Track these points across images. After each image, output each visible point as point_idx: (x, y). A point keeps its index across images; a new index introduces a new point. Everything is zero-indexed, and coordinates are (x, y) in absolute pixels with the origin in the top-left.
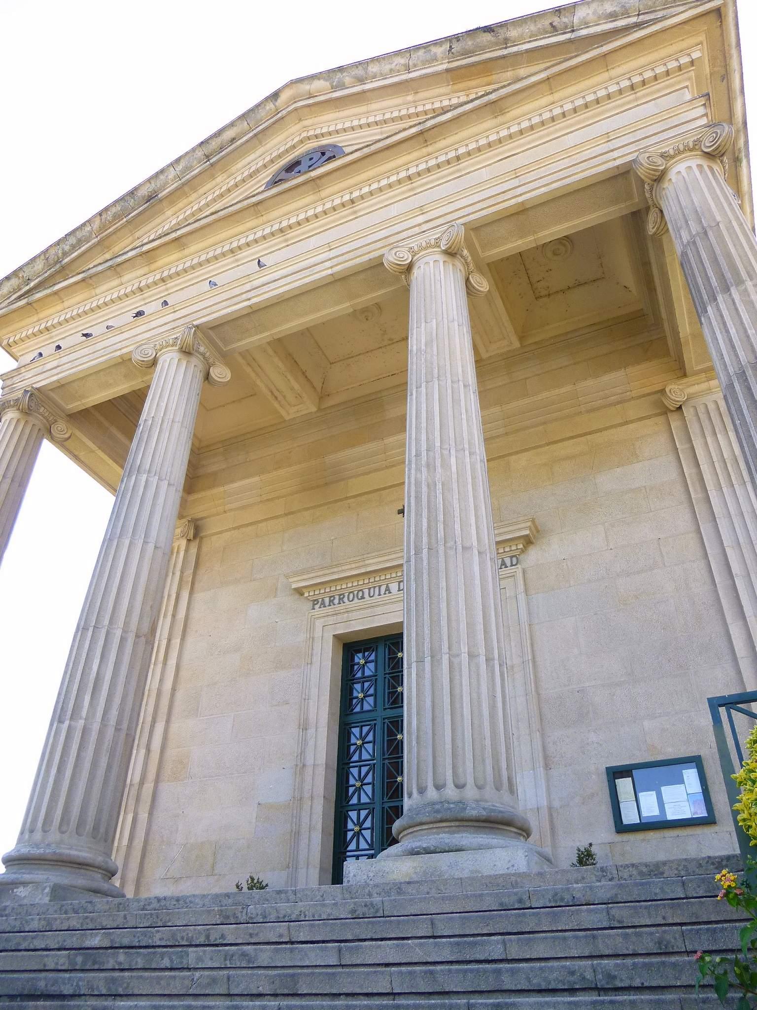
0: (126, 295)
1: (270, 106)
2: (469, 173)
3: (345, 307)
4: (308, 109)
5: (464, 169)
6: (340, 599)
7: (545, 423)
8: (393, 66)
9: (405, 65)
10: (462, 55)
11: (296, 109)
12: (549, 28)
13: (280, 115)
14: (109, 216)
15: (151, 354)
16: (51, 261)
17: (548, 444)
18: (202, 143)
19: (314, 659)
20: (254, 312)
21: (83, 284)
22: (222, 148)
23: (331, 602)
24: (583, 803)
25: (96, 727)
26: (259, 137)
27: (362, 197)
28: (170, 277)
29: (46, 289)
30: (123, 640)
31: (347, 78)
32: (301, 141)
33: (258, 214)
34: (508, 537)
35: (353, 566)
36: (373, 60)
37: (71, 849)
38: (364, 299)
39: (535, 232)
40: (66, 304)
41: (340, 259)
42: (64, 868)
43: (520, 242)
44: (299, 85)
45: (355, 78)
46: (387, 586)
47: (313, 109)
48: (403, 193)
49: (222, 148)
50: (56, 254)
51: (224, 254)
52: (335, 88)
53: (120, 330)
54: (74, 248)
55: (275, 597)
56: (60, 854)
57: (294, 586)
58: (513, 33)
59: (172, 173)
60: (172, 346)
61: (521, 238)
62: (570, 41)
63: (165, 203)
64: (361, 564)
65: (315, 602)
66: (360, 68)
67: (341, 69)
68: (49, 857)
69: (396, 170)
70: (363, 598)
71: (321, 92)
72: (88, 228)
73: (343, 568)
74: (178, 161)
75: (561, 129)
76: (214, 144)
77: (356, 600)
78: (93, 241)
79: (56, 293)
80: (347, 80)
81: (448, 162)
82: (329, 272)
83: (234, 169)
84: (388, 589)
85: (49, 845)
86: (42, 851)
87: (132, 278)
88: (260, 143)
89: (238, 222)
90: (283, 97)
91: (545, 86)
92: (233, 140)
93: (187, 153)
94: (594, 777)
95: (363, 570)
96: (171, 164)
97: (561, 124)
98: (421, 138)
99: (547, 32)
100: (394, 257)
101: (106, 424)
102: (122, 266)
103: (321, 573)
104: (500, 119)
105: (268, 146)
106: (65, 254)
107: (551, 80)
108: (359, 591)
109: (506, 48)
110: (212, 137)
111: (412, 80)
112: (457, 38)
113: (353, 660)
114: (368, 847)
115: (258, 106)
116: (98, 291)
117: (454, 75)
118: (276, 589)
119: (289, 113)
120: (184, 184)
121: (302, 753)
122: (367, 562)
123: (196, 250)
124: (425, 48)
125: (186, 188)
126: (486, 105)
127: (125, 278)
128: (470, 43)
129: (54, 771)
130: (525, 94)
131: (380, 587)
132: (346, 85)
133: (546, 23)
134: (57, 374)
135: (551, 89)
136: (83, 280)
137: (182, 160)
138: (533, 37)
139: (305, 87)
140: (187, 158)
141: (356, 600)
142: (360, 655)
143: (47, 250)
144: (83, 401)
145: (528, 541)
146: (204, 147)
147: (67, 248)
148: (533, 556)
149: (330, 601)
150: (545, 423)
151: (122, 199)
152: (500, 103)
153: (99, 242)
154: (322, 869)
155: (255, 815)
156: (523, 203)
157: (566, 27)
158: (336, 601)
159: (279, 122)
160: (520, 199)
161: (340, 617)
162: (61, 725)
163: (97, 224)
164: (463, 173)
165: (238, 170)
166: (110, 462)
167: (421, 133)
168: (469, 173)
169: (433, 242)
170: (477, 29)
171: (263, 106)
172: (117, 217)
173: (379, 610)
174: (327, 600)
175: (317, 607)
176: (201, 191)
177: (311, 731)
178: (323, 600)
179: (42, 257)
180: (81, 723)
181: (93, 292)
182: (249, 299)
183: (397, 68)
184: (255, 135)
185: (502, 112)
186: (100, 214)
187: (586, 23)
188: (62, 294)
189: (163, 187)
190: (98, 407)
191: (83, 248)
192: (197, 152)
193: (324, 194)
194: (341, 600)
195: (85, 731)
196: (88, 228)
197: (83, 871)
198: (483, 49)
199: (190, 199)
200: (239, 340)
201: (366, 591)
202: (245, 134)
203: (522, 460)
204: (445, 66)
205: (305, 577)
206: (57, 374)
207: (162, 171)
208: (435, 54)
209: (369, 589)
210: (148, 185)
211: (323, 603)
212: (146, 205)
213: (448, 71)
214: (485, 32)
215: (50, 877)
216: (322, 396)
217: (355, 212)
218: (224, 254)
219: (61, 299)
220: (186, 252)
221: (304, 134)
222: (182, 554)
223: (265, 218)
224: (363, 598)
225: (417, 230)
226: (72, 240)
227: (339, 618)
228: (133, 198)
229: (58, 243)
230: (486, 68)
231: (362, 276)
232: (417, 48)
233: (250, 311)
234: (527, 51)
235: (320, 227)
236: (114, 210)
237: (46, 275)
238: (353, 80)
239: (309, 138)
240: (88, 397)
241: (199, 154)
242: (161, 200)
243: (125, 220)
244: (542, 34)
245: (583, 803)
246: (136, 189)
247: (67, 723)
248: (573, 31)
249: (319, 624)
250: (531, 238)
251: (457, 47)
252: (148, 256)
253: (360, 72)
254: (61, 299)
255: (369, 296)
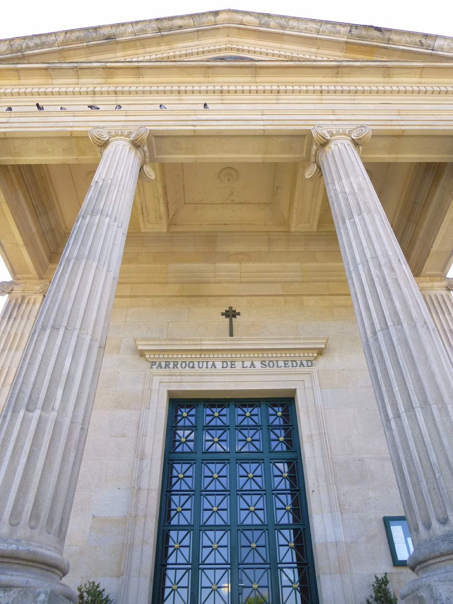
0: (80, 93)
1: (211, 18)
2: (360, 104)
3: (257, 157)
4: (237, 30)
5: (358, 100)
6: (174, 365)
7: (328, 281)
8: (308, 26)
9: (317, 29)
10: (358, 37)
11: (229, 27)
12: (419, 43)
13: (217, 26)
14: (74, 36)
15: (106, 137)
16: (14, 48)
17: (330, 295)
18: (158, 19)
19: (151, 405)
20: (196, 136)
21: (44, 72)
22: (171, 29)
23: (167, 366)
24: (368, 542)
25: (67, 421)
26: (200, 33)
27: (286, 92)
28: (123, 93)
29: (9, 64)
30: (90, 347)
31: (273, 22)
32: (226, 49)
33: (206, 75)
34: (310, 346)
35: (191, 343)
36: (294, 18)
37: (41, 547)
38: (274, 156)
39: (398, 153)
40: (22, 82)
41: (271, 123)
42: (34, 569)
43: (387, 156)
44: (234, 14)
45: (278, 23)
46: (213, 363)
47: (241, 32)
48: (314, 99)
49: (171, 29)
50: (21, 45)
51: (172, 92)
52: (260, 25)
53: (74, 114)
54: (37, 46)
55: (117, 353)
56: (34, 553)
57: (140, 348)
58: (394, 37)
59: (130, 29)
60: (126, 137)
61: (389, 153)
62: (431, 55)
63: (119, 46)
64: (197, 342)
65: (153, 363)
66: (283, 19)
67: (269, 15)
68: (23, 556)
69: (313, 84)
70: (193, 367)
71: (249, 24)
72: (53, 38)
73: (183, 343)
74: (137, 23)
75: (421, 100)
76: (166, 24)
77: (187, 368)
78: (55, 48)
79: (17, 70)
80: (272, 23)
81: (349, 92)
82: (262, 128)
83: (175, 46)
84: (214, 365)
85: (18, 541)
86: (14, 547)
87: (88, 83)
88: (198, 38)
89: (189, 74)
90: (222, 17)
91: (419, 71)
92: (180, 27)
93: (144, 21)
94: (374, 523)
95: (199, 347)
96: (132, 23)
97: (422, 97)
98: (336, 71)
99: (416, 45)
100: (323, 131)
101: (17, 186)
102: (85, 71)
103: (164, 343)
104: (387, 80)
105: (203, 42)
106: (28, 48)
107: (424, 69)
108: (190, 362)
109: (388, 44)
110: (165, 19)
111: (320, 39)
112: (357, 26)
113: (177, 412)
114: (284, 570)
115: (203, 14)
116: (55, 81)
117: (348, 47)
118: (119, 348)
119: (224, 28)
120: (138, 39)
121: (139, 477)
122: (203, 342)
123: (148, 81)
124: (333, 24)
125: (138, 43)
126: (383, 67)
127: (82, 81)
128: (364, 33)
129: (23, 460)
130: (407, 71)
131: (207, 362)
132: (266, 27)
133: (417, 39)
134: (5, 128)
135: (421, 75)
136: (46, 69)
137: (140, 24)
138: (406, 44)
139: (239, 17)
140: (144, 23)
141: (187, 368)
142: (183, 410)
143: (13, 39)
144: (16, 158)
145: (320, 352)
146: (158, 22)
147: (31, 44)
148: (322, 363)
149: (166, 365)
150: (328, 281)
151: (87, 29)
152: (391, 69)
153: (60, 50)
154: (151, 578)
155: (89, 526)
156: (404, 130)
157: (429, 46)
158: (171, 365)
159: (214, 30)
160: (403, 128)
161: (174, 378)
162: (30, 414)
163: (61, 38)
164: (356, 102)
165: (177, 48)
166: (9, 215)
167: (338, 67)
168: (360, 104)
169: (347, 132)
170: (371, 26)
171: (206, 15)
172: (79, 40)
173: (186, 379)
174: (163, 364)
175: (155, 367)
176: (148, 50)
177: (147, 462)
178: (160, 363)
179: (7, 42)
180: (54, 414)
181: (50, 81)
182: (194, 126)
183: (311, 29)
184: (198, 31)
185: (389, 76)
186: (66, 32)
187: (442, 49)
188: (21, 73)
189: (121, 35)
190: (19, 168)
191: (45, 50)
192: (152, 23)
193: (258, 79)
194: (175, 366)
195: (57, 424)
196: (53, 38)
197: (50, 573)
198: (372, 39)
199: (138, 51)
200: (170, 154)
201: (196, 364)
202: (190, 27)
203: (311, 301)
204: (345, 40)
205: (151, 343)
206: (5, 128)
207: (123, 24)
208: (339, 31)
209: (199, 362)
210: (110, 29)
211: (160, 365)
212: (104, 41)
213: (346, 43)
214: (375, 30)
215: (30, 580)
216: (171, 224)
217: (278, 99)
218: (172, 92)
219: (19, 76)
220: (141, 80)
221: (228, 46)
222: (38, 305)
223: (210, 79)
224: (193, 367)
225: (330, 122)
226: (37, 41)
227: (174, 378)
228: (96, 32)
229: (24, 38)
230: (372, 50)
231: (281, 140)
232: (327, 22)
233: (193, 134)
234: (403, 50)
235: (251, 100)
236: (78, 34)
237: (8, 56)
238: (277, 25)
239: (232, 49)
240: (22, 156)
241: (154, 25)
242: (117, 42)
243: (85, 44)
244: (413, 44)
245: (368, 542)
246: (100, 27)
247: (38, 412)
248: (433, 50)
249: (156, 380)
250: (393, 156)
251: (354, 31)
252: (109, 71)
253: (283, 22)
254: (19, 76)
255: (278, 156)
